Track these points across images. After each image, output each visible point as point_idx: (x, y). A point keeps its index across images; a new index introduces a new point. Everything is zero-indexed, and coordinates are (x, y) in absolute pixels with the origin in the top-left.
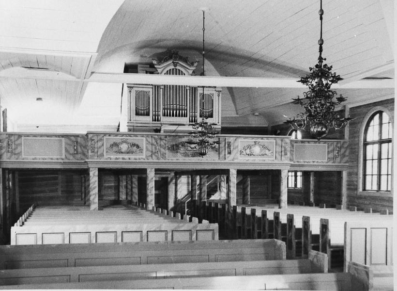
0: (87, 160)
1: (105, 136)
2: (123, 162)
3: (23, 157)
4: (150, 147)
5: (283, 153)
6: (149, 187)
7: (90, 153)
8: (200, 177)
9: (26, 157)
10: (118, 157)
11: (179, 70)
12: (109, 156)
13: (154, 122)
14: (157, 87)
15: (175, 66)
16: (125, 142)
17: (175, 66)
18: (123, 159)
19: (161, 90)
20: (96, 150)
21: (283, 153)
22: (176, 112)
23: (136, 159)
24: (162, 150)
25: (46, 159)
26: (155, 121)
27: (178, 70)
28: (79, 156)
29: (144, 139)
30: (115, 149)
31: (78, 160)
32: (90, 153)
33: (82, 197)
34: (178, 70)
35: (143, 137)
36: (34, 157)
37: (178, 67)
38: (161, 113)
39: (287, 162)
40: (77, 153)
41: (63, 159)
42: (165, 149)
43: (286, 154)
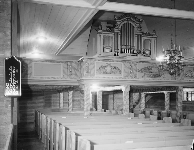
1: (95, 60)
2: (108, 80)
3: (33, 76)
4: (127, 70)
6: (142, 97)
7: (85, 73)
9: (35, 76)
10: (104, 76)
11: (130, 24)
12: (98, 76)
13: (115, 56)
14: (117, 34)
15: (128, 21)
16: (108, 65)
17: (128, 21)
18: (108, 78)
19: (120, 36)
20: (89, 71)
22: (128, 51)
23: (117, 78)
24: (135, 72)
25: (50, 78)
26: (116, 55)
27: (130, 24)
28: (73, 76)
29: (122, 63)
30: (102, 70)
31: (72, 79)
32: (85, 73)
34: (131, 25)
35: (122, 62)
36: (41, 77)
37: (130, 22)
38: (120, 51)
41: (62, 79)
42: (136, 71)
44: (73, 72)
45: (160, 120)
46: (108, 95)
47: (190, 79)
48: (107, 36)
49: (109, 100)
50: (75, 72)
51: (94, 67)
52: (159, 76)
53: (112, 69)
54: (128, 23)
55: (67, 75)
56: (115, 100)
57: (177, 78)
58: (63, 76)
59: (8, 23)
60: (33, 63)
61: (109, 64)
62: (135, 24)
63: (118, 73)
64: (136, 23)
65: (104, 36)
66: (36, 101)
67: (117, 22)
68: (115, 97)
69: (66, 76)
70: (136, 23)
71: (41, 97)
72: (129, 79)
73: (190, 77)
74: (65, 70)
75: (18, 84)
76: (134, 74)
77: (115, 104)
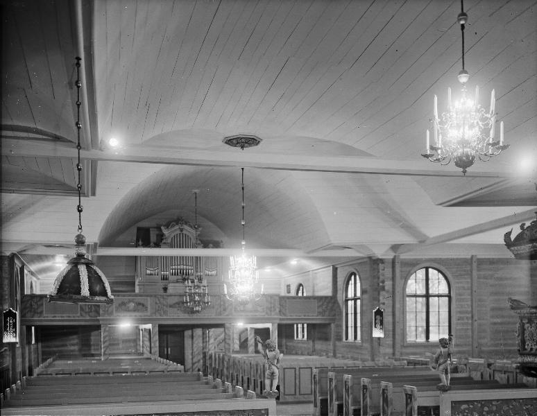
0: (98, 318)
3: (45, 315)
5: (273, 309)
8: (396, 331)
21: (273, 309)
30: (123, 307)
33: (471, 275)
39: (276, 317)
40: (91, 312)
42: (167, 306)
43: (275, 310)
46: (183, 331)
49: (186, 339)
52: (487, 279)
55: (86, 313)
56: (195, 339)
58: (81, 313)
59: (24, 152)
66: (68, 343)
68: (194, 335)
69: (84, 314)
71: (75, 337)
75: (15, 332)
77: (195, 345)
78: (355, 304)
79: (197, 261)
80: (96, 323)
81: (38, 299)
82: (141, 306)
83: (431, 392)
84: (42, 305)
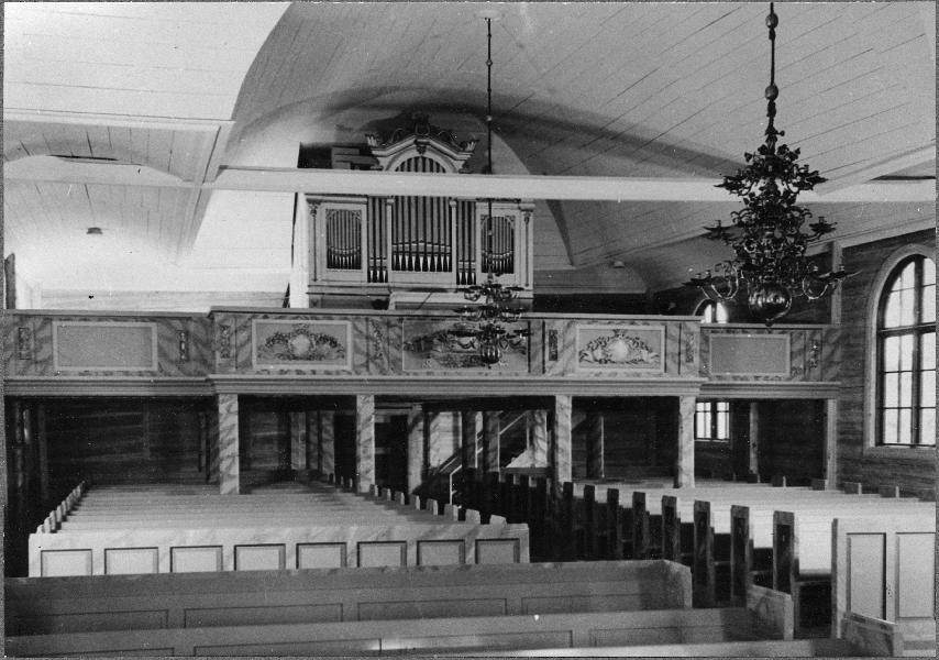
0: (211, 376)
1: (254, 317)
3: (57, 368)
4: (362, 344)
5: (683, 358)
7: (219, 359)
9: (64, 369)
10: (285, 367)
11: (431, 161)
12: (264, 367)
14: (377, 201)
19: (389, 208)
20: (233, 352)
21: (683, 358)
22: (410, 260)
24: (393, 351)
25: (111, 374)
28: (192, 366)
29: (349, 324)
30: (279, 348)
31: (190, 375)
32: (219, 359)
34: (428, 162)
36: (83, 369)
37: (428, 155)
38: (388, 263)
39: (692, 378)
40: (188, 360)
43: (690, 360)
44: (193, 351)
45: (6, 576)
47: (597, 371)
48: (341, 211)
50: (200, 352)
51: (249, 339)
53: (314, 343)
54: (420, 160)
57: (547, 369)
60: (56, 323)
61: (301, 327)
62: (447, 161)
63: (334, 355)
64: (451, 157)
65: (329, 211)
67: (379, 159)
69: (166, 366)
70: (451, 157)
72: (371, 374)
73: (600, 361)
74: (165, 345)
76: (391, 358)
78: (417, 237)
79: (435, 205)
80: (208, 392)
81: (39, 322)
82: (326, 346)
83: (710, 646)
84: (50, 338)
